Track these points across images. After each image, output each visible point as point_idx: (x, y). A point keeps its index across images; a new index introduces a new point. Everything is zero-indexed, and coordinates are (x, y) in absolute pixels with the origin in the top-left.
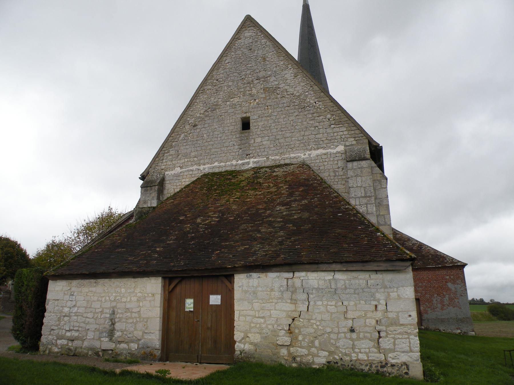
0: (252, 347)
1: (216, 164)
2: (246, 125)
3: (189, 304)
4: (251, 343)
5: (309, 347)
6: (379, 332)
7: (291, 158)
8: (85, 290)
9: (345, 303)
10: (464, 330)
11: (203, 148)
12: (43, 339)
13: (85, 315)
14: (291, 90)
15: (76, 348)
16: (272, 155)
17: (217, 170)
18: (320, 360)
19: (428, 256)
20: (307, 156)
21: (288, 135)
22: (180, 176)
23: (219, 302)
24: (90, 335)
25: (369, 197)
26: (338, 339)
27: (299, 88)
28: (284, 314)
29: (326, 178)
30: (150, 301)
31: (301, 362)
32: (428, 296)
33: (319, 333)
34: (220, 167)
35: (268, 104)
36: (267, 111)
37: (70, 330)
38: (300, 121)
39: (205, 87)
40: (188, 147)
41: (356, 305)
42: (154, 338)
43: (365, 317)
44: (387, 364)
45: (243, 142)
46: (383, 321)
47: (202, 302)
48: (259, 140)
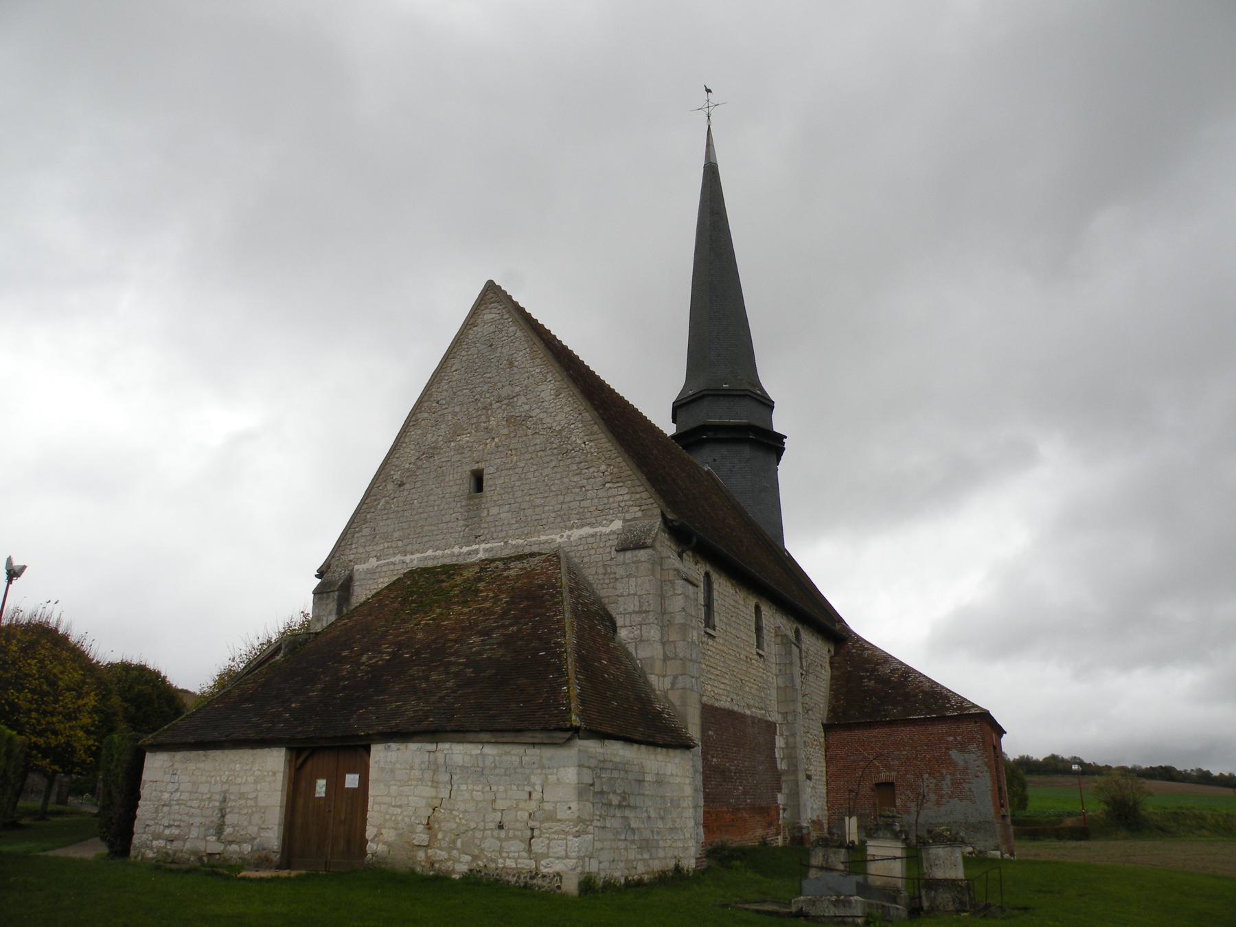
0: (385, 848)
1: (430, 553)
2: (478, 480)
3: (321, 787)
4: (385, 843)
5: (450, 849)
6: (532, 829)
7: (540, 543)
8: (192, 766)
9: (494, 788)
10: (980, 846)
11: (412, 524)
12: (136, 840)
13: (189, 803)
14: (548, 420)
15: (175, 852)
16: (514, 537)
17: (430, 564)
18: (461, 866)
19: (916, 695)
20: (565, 539)
21: (538, 502)
22: (375, 573)
23: (356, 785)
24: (194, 833)
25: (646, 612)
26: (483, 838)
27: (561, 416)
28: (424, 802)
29: (591, 578)
30: (270, 783)
31: (439, 870)
32: (911, 777)
33: (462, 829)
34: (435, 558)
35: (512, 446)
36: (509, 460)
37: (169, 826)
38: (558, 476)
39: (419, 416)
40: (389, 522)
41: (506, 791)
42: (272, 837)
43: (517, 808)
44: (537, 874)
45: (472, 514)
46: (537, 814)
47: (336, 784)
48: (494, 511)
